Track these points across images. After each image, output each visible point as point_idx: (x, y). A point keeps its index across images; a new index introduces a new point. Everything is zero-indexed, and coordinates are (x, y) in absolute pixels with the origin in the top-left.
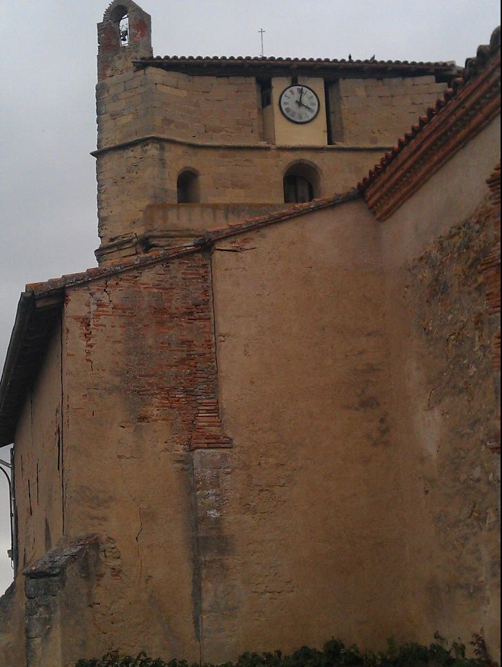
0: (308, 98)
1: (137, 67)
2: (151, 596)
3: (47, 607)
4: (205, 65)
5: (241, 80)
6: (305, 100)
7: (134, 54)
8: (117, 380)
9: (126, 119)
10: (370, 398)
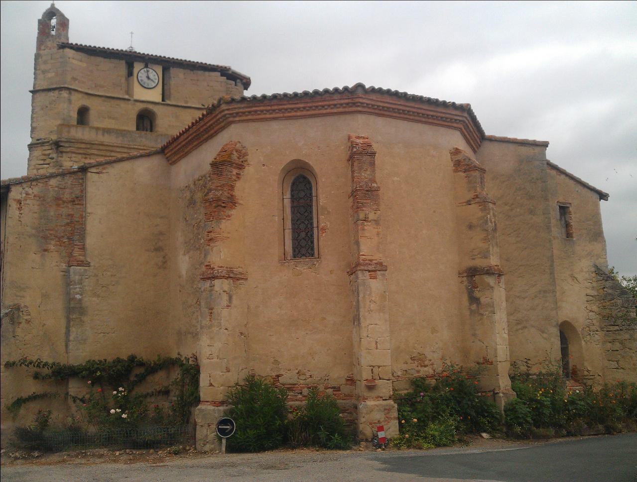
0: (152, 74)
4: (98, 51)
6: (151, 76)
7: (58, 40)
8: (34, 232)
10: (159, 247)
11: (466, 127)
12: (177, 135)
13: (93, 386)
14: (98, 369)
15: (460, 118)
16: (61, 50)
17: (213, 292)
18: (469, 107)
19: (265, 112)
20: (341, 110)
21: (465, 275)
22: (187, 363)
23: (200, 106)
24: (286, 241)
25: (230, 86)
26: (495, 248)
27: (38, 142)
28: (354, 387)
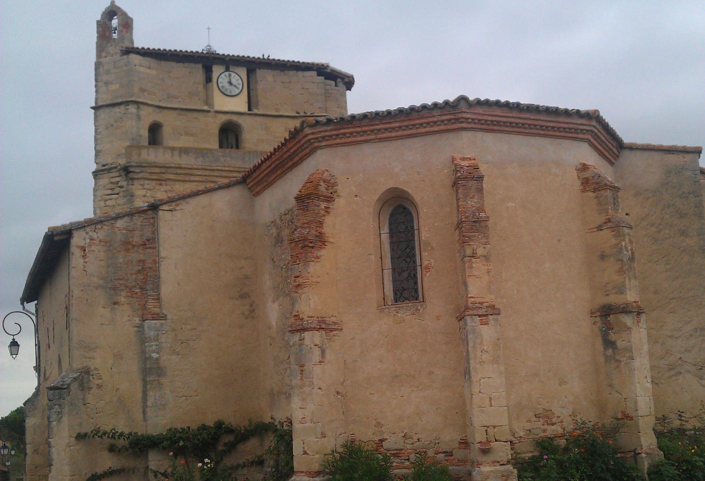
0: (235, 79)
1: (123, 53)
2: (119, 399)
3: (60, 405)
4: (169, 54)
5: (193, 65)
6: (234, 81)
8: (101, 282)
9: (115, 87)
10: (245, 294)
11: (596, 137)
12: (258, 163)
13: (176, 458)
14: (181, 438)
15: (588, 128)
16: (125, 57)
17: (303, 346)
18: (597, 114)
19: (354, 134)
20: (442, 127)
21: (598, 314)
22: (281, 428)
23: (295, 114)
24: (385, 283)
25: (329, 87)
26: (633, 281)
27: (103, 168)
28: (468, 451)
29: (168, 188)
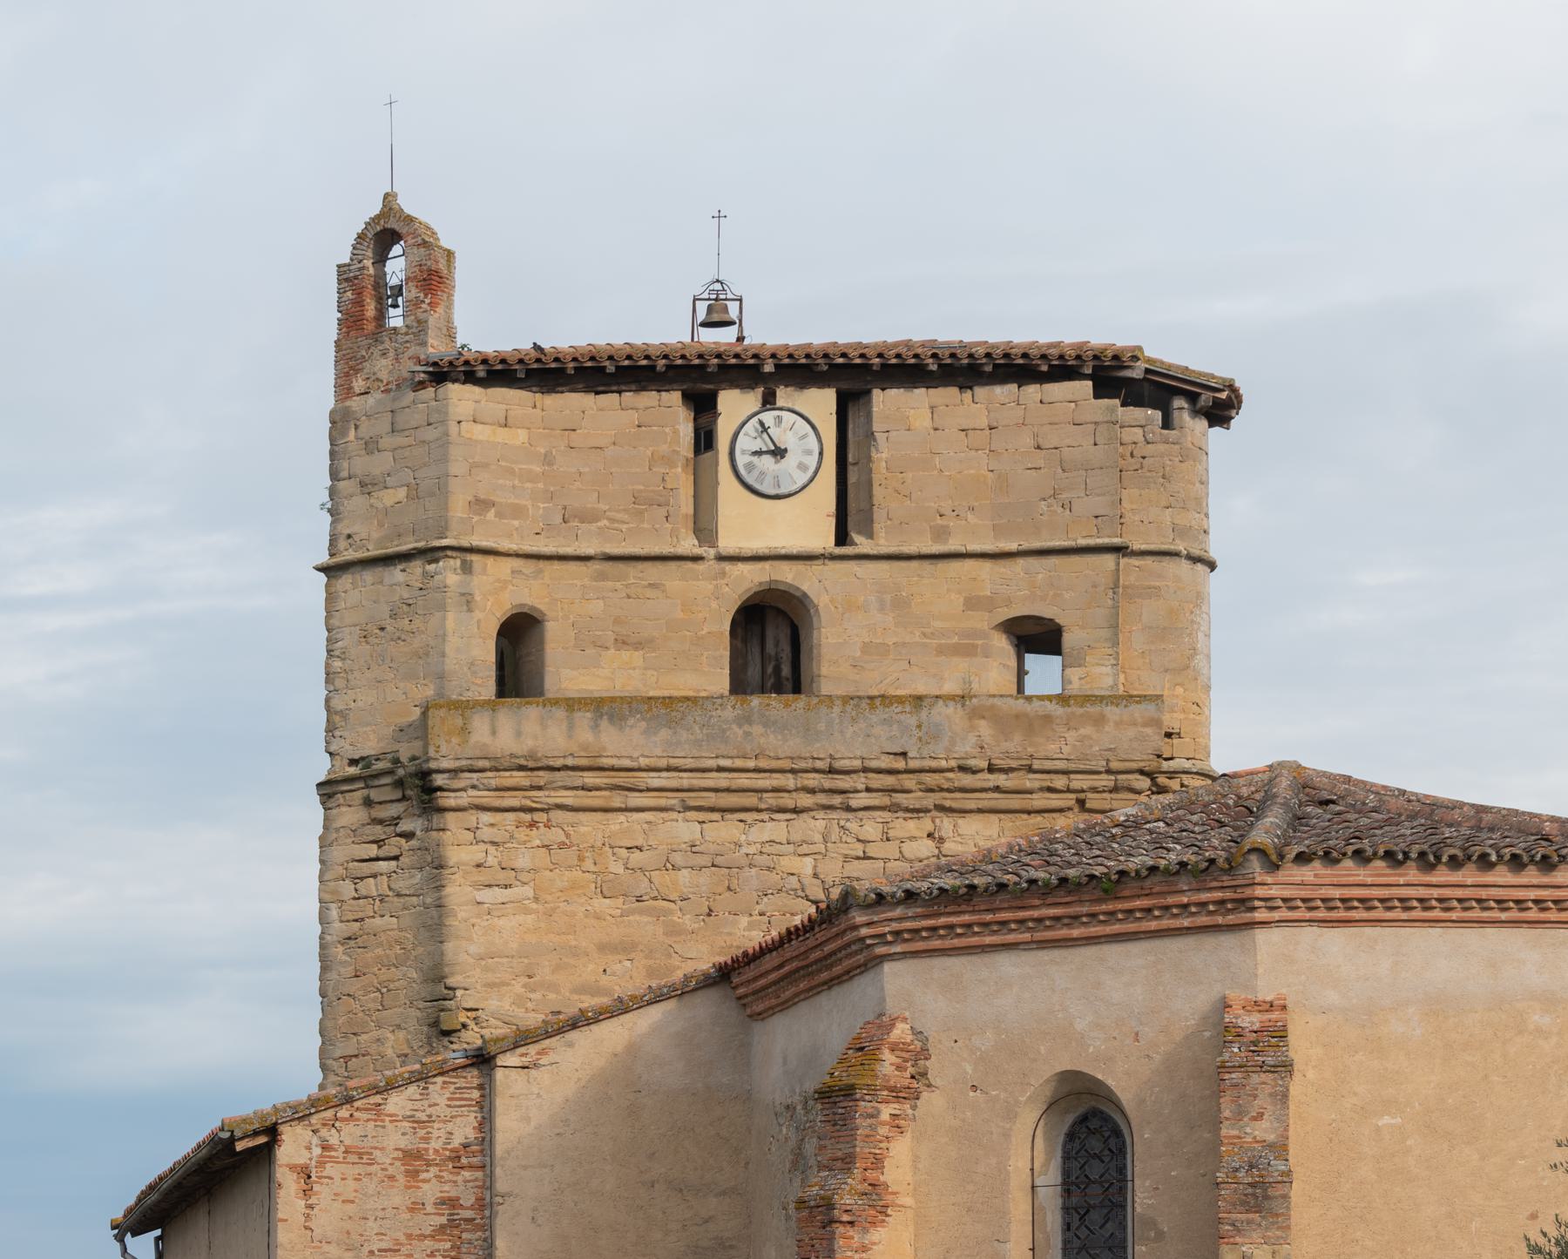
5: (649, 398)
7: (413, 350)
29: (556, 835)
